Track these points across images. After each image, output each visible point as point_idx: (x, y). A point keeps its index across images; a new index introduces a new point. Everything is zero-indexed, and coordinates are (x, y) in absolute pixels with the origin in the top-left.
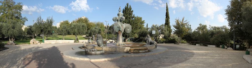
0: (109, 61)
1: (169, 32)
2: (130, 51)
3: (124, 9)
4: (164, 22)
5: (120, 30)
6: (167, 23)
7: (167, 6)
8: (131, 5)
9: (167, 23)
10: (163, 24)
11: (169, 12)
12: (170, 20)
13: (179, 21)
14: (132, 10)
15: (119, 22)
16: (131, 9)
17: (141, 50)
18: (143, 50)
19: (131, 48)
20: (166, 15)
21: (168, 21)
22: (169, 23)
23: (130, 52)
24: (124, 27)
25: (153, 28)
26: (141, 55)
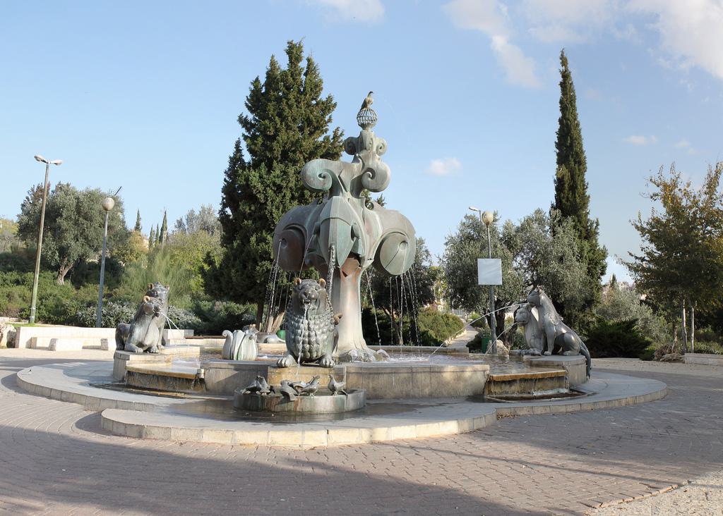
0: (476, 433)
1: (589, 272)
2: (490, 392)
3: (263, 80)
4: (545, 198)
5: (360, 252)
6: (570, 197)
7: (565, 75)
8: (315, 60)
9: (570, 197)
10: (538, 212)
11: (579, 118)
12: (588, 177)
13: (680, 195)
14: (323, 97)
15: (348, 195)
16: (317, 87)
17: (539, 385)
18: (550, 384)
19: (492, 369)
20: (558, 145)
21: (573, 188)
22: (585, 200)
23: (487, 397)
24: (381, 232)
25: (475, 238)
26: (578, 408)
